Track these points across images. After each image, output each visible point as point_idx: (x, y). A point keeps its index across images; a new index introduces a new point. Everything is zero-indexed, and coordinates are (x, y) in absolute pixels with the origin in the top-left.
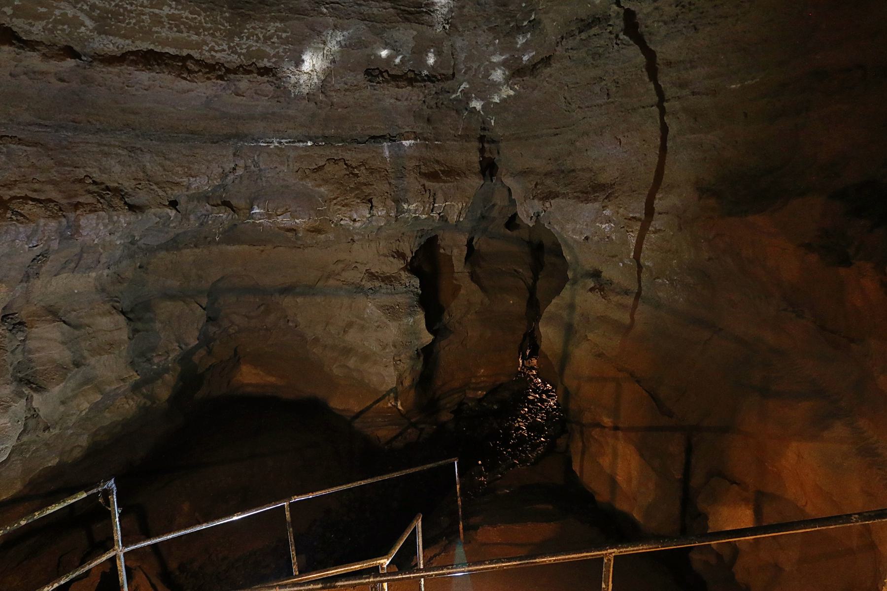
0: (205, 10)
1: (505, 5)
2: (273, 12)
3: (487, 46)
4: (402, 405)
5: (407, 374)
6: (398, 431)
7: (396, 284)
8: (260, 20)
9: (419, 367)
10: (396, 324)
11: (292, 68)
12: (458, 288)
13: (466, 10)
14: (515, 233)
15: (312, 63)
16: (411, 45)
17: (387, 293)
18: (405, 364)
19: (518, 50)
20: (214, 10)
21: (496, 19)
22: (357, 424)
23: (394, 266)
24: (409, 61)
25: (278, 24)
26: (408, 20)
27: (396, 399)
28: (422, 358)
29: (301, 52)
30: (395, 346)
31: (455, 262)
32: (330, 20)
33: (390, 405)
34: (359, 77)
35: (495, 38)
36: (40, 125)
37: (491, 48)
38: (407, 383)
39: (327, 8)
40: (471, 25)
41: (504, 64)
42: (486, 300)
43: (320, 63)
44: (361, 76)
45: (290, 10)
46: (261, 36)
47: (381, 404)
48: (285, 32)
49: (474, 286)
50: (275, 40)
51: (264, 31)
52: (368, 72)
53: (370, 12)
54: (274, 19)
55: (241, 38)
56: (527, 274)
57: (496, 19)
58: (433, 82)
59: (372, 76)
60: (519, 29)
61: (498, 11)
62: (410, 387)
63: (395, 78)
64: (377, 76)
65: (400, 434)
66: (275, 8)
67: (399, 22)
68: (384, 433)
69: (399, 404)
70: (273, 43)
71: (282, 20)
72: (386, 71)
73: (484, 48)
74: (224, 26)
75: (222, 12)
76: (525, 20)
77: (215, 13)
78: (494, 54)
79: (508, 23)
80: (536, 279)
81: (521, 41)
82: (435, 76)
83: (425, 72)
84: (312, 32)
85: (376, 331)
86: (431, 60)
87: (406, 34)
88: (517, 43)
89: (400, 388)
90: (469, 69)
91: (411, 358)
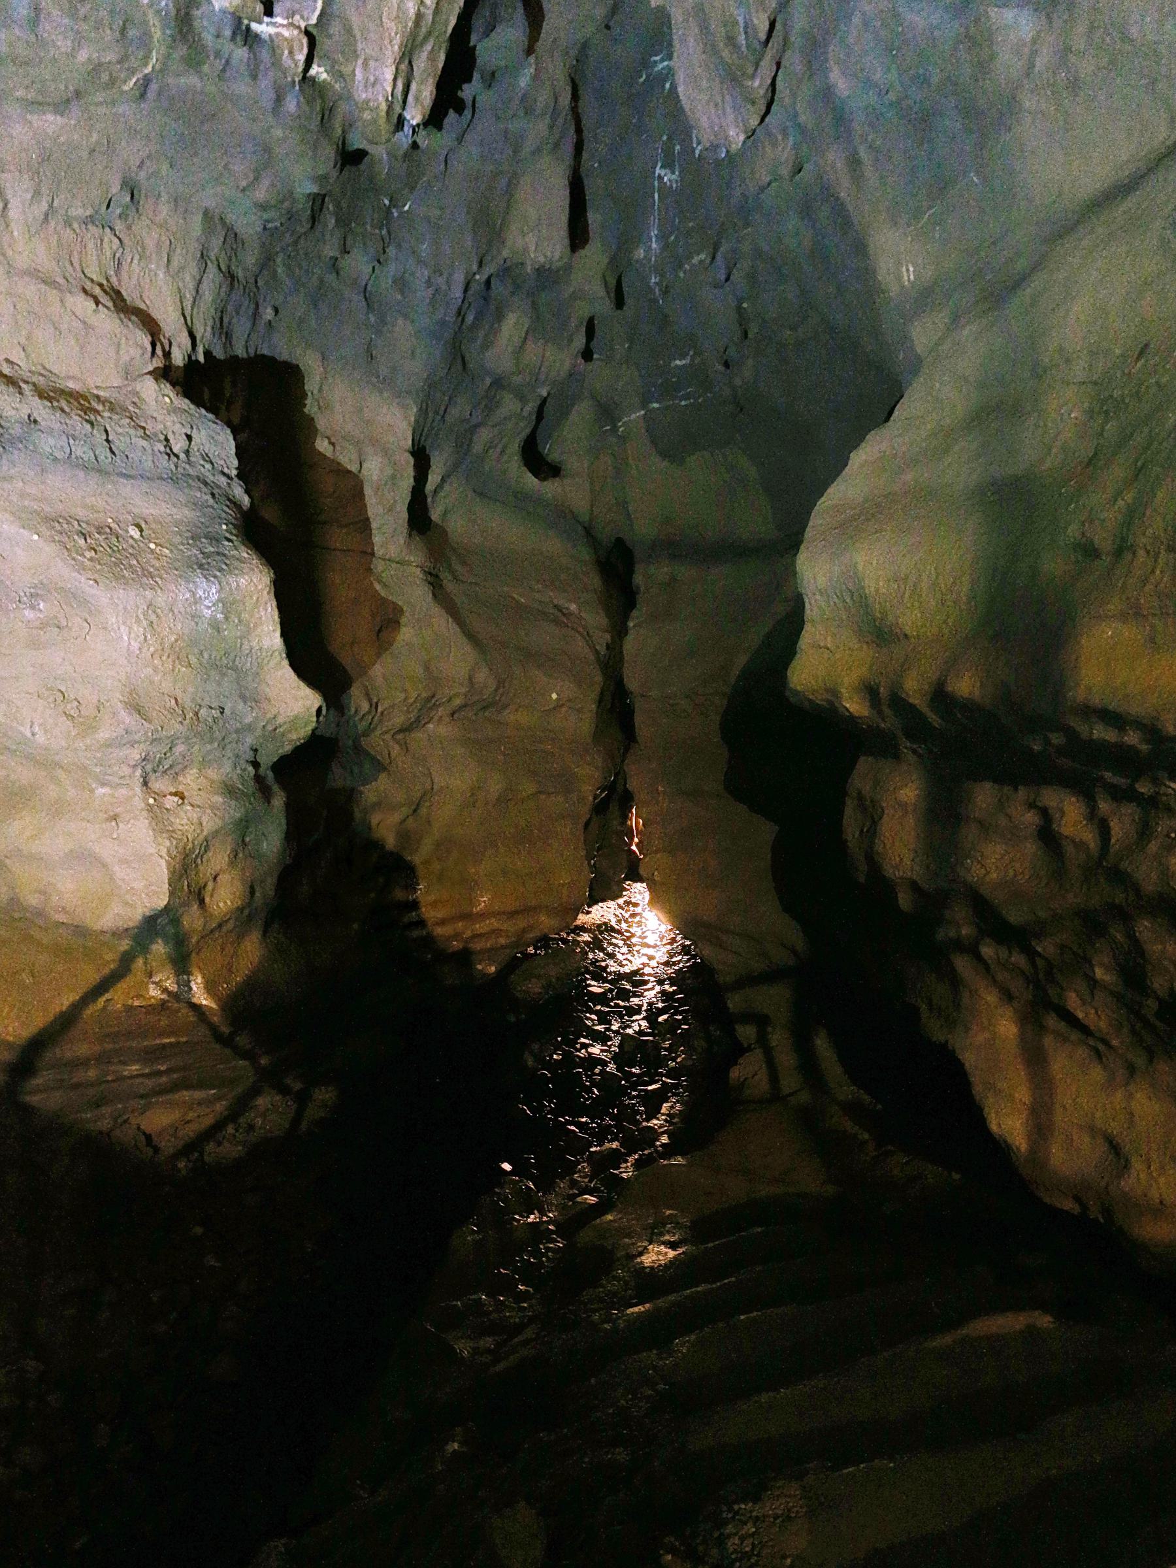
4: (210, 987)
5: (218, 859)
6: (220, 1107)
7: (121, 431)
9: (271, 840)
10: (130, 598)
12: (387, 620)
14: (550, 489)
17: (71, 461)
18: (202, 804)
22: (43, 1094)
23: (107, 356)
27: (181, 963)
28: (279, 800)
30: (137, 709)
31: (374, 507)
33: (154, 992)
38: (225, 898)
42: (482, 675)
47: (118, 997)
49: (442, 622)
56: (596, 620)
62: (244, 917)
65: (233, 1116)
68: (168, 1119)
69: (197, 984)
80: (619, 631)
85: (34, 644)
89: (192, 920)
91: (230, 791)
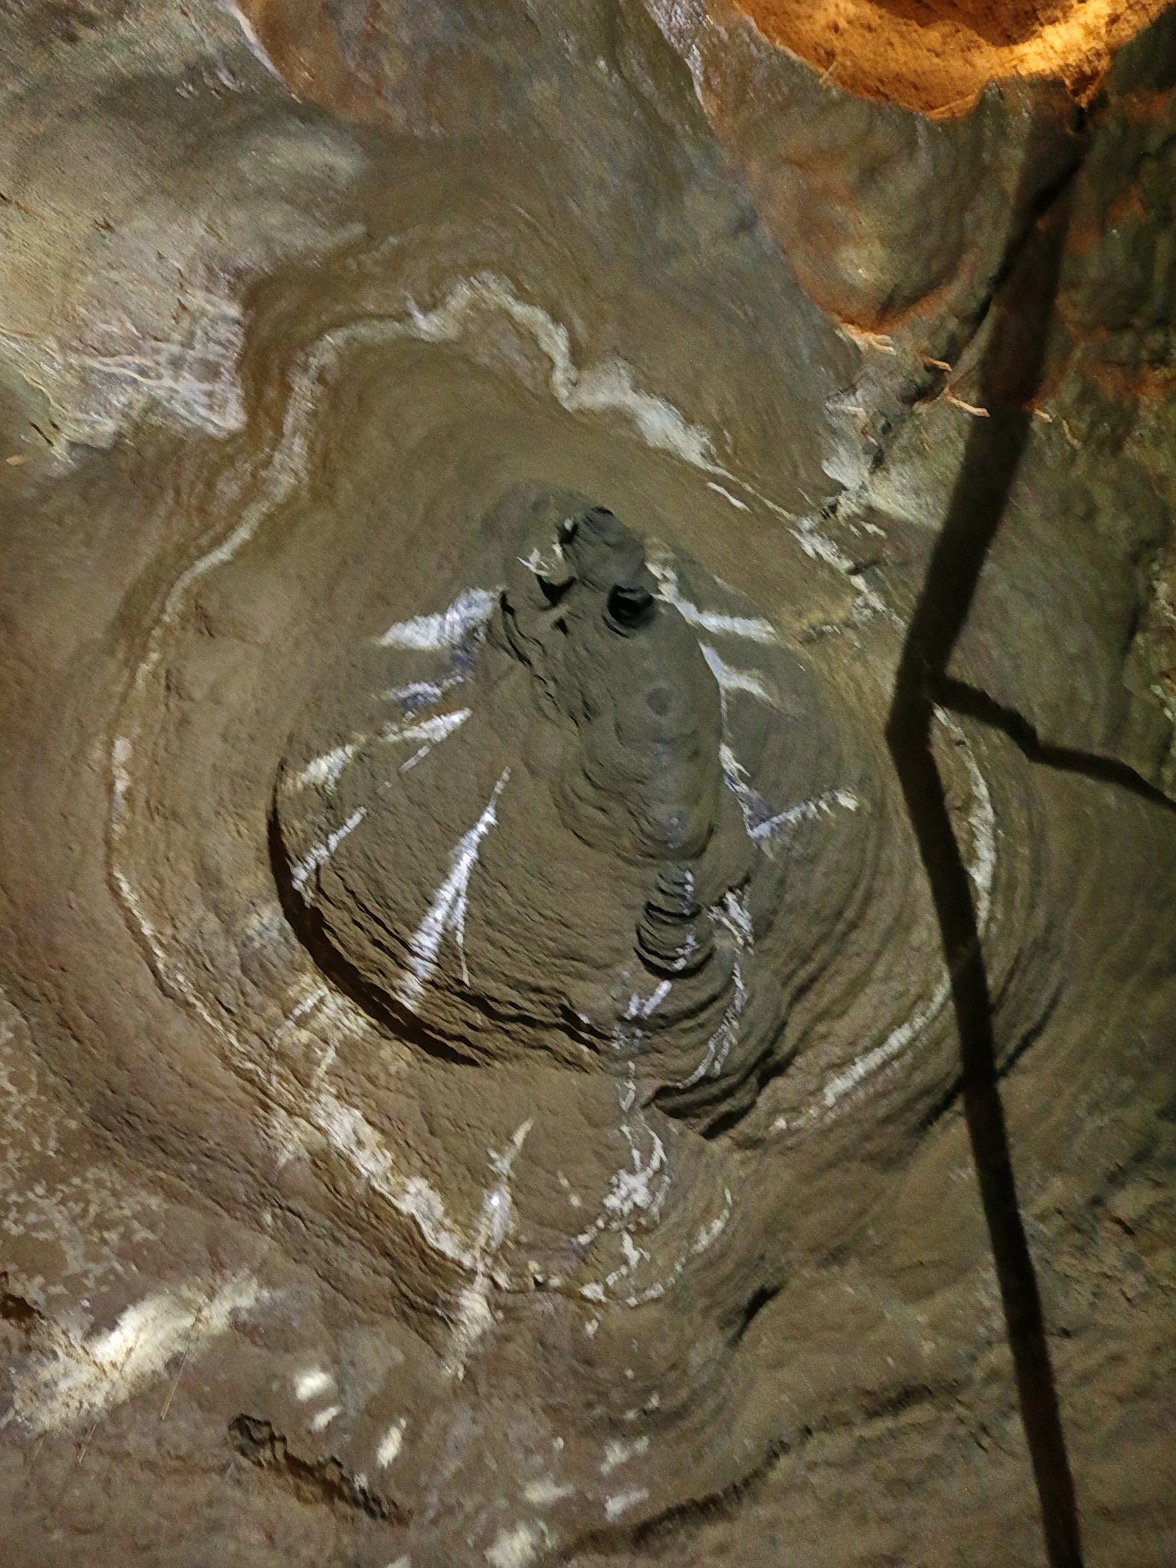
0: (44, 1088)
1: (589, 1363)
2: (165, 1168)
3: (528, 1452)
8: (127, 1173)
11: (76, 1335)
13: (511, 1347)
15: (136, 1341)
16: (373, 1388)
19: (600, 1479)
20: (58, 1097)
21: (566, 1388)
24: (345, 1431)
25: (155, 1202)
26: (406, 1317)
29: (135, 1297)
32: (264, 1244)
34: (209, 1433)
35: (555, 1434)
36: (360, 904)
37: (538, 1460)
39: (274, 1216)
40: (510, 1384)
41: (554, 1513)
43: (149, 1349)
44: (216, 1430)
45: (204, 1184)
46: (93, 1210)
48: (152, 1227)
50: (112, 1236)
51: (111, 1201)
52: (242, 1424)
53: (345, 1268)
54: (156, 1185)
55: (51, 1191)
57: (566, 1388)
58: (372, 1513)
59: (251, 1438)
60: (616, 1428)
61: (575, 1372)
63: (296, 1466)
64: (260, 1443)
66: (173, 1163)
67: (388, 1314)
70: (104, 1241)
71: (171, 1195)
72: (283, 1439)
73: (520, 1456)
74: (44, 1145)
75: (70, 1114)
76: (629, 1406)
77: (57, 1107)
78: (538, 1476)
79: (590, 1405)
81: (616, 1454)
82: (378, 1502)
83: (361, 1481)
84: (205, 1255)
86: (389, 1449)
87: (380, 1349)
88: (603, 1458)
90: (449, 1511)
